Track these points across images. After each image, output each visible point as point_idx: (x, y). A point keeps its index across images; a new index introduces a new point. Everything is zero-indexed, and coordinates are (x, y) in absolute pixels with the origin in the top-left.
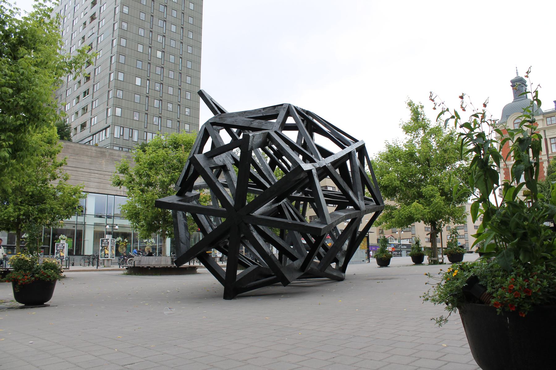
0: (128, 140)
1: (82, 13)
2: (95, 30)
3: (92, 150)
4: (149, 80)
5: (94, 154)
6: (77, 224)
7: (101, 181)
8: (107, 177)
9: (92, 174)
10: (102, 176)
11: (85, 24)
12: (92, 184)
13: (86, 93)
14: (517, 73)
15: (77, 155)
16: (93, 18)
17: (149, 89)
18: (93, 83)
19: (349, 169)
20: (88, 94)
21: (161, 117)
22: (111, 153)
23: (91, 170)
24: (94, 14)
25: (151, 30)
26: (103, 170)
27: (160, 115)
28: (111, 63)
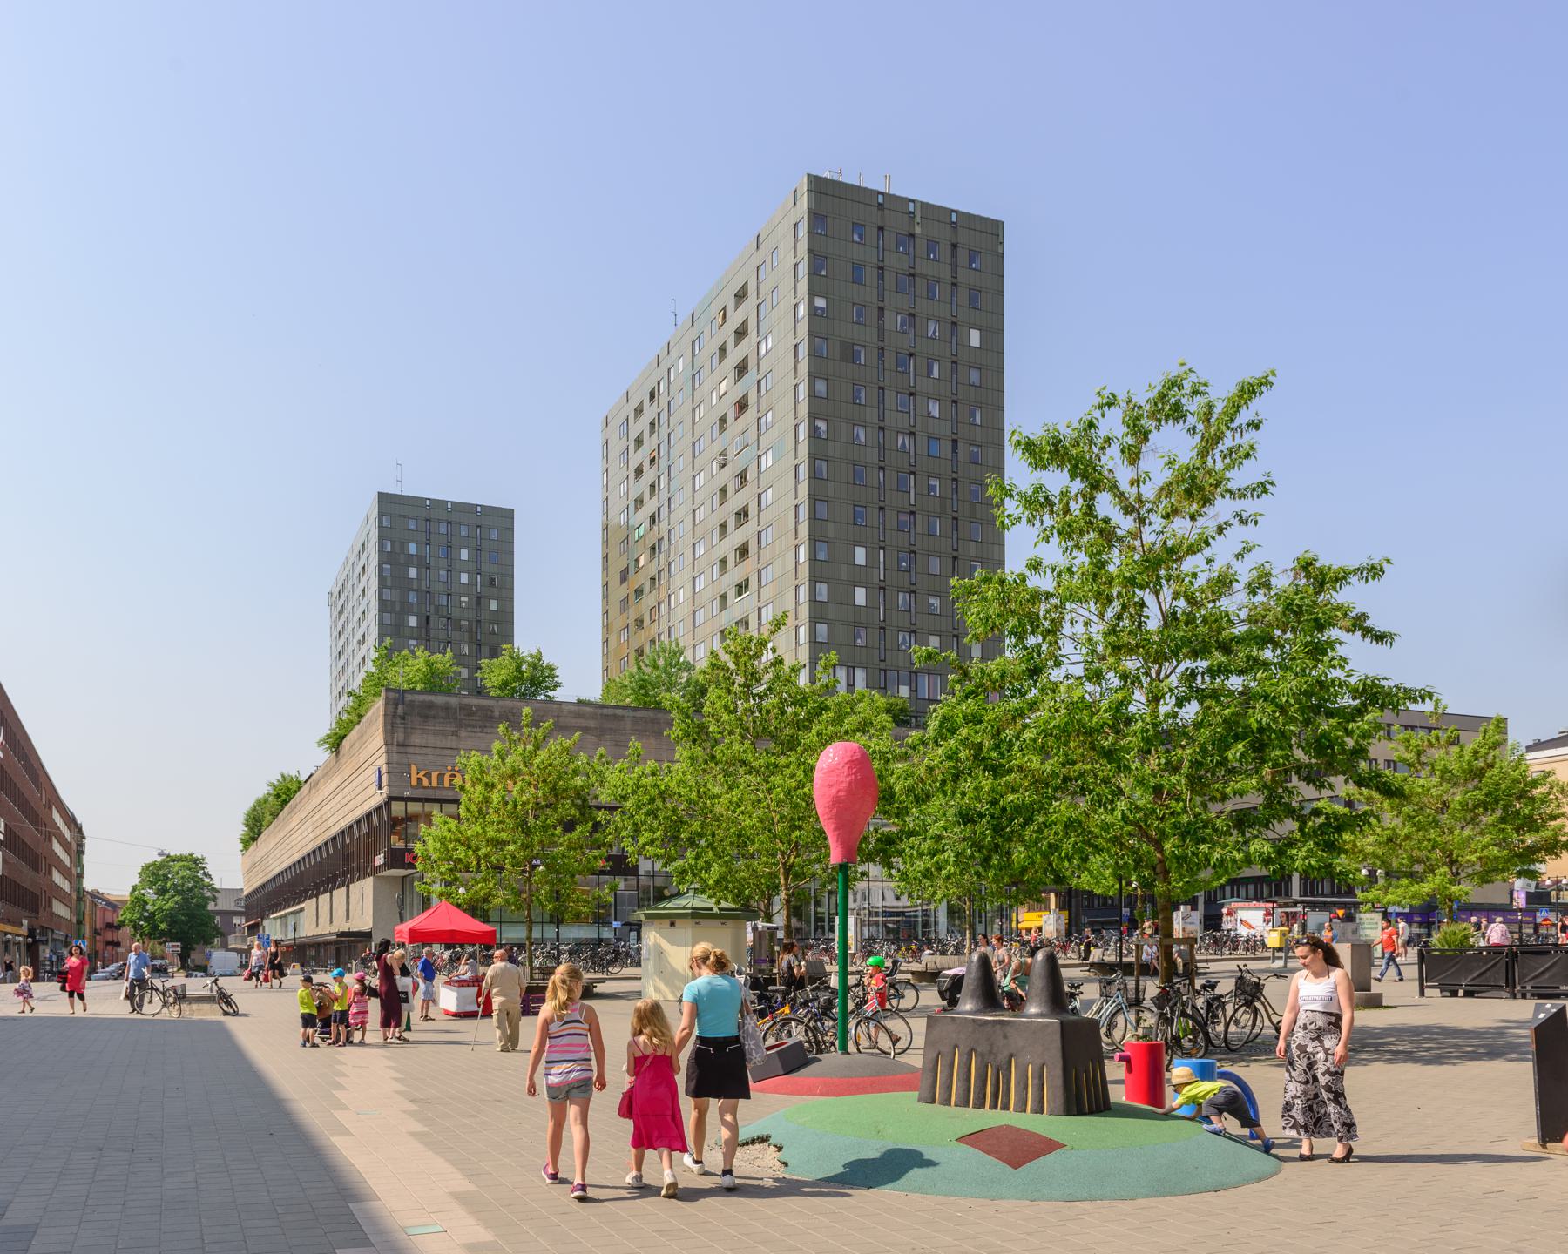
1: (714, 463)
2: (752, 435)
4: (883, 548)
11: (723, 420)
13: (741, 588)
14: (1413, 980)
16: (742, 406)
17: (885, 569)
18: (756, 416)
20: (746, 590)
21: (915, 592)
24: (745, 397)
25: (882, 424)
27: (913, 628)
28: (796, 442)
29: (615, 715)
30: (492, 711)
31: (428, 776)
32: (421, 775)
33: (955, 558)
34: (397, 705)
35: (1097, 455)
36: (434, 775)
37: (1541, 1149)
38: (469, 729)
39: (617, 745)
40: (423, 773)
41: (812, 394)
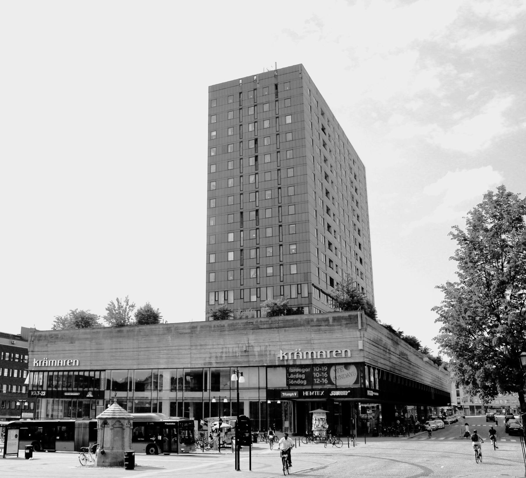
0: (297, 298)
3: (160, 328)
5: (161, 333)
6: (230, 389)
7: (169, 357)
8: (174, 351)
9: (161, 351)
10: (170, 351)
12: (162, 361)
15: (147, 335)
19: (296, 405)
22: (176, 327)
23: (160, 348)
26: (169, 346)
29: (97, 332)
30: (58, 336)
31: (38, 362)
32: (284, 355)
33: (242, 250)
34: (32, 337)
35: (462, 234)
36: (290, 354)
37: (130, 450)
38: (51, 343)
39: (97, 344)
40: (285, 353)
41: (210, 156)
